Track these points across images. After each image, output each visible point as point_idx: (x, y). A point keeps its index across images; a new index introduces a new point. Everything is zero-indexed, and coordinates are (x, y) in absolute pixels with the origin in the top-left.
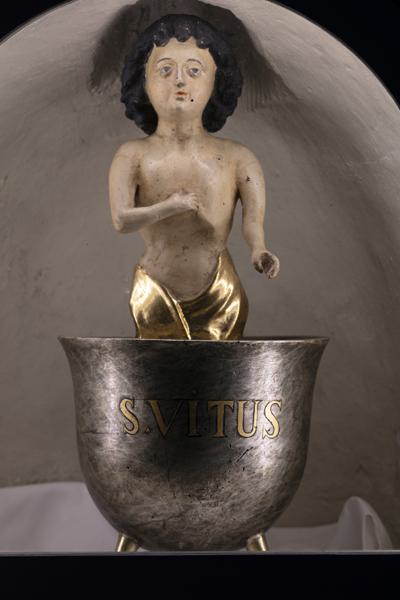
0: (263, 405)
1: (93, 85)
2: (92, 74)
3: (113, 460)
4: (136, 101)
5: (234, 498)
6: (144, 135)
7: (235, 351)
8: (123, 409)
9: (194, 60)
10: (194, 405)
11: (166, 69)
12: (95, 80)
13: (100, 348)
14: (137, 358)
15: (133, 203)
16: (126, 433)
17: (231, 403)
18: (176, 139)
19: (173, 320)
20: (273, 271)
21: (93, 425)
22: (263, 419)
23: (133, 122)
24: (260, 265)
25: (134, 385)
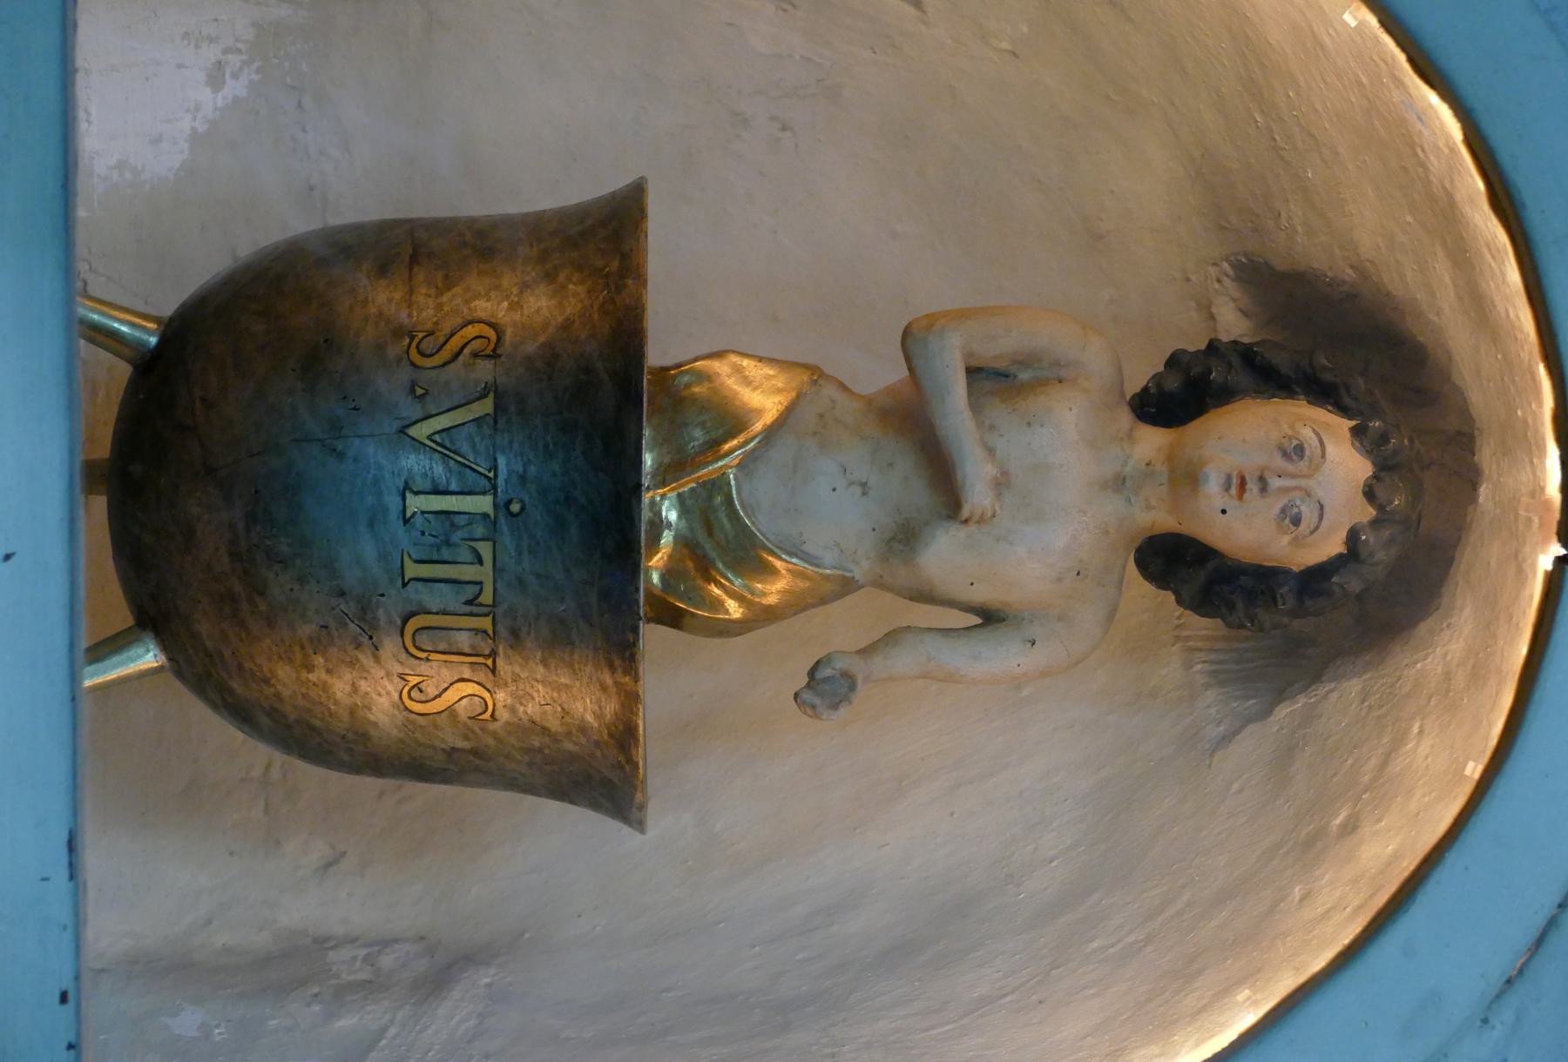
0: (481, 676)
1: (1237, 266)
2: (1267, 264)
6: (1135, 385)
8: (471, 331)
14: (599, 365)
15: (974, 363)
16: (412, 338)
21: (430, 255)
22: (447, 675)
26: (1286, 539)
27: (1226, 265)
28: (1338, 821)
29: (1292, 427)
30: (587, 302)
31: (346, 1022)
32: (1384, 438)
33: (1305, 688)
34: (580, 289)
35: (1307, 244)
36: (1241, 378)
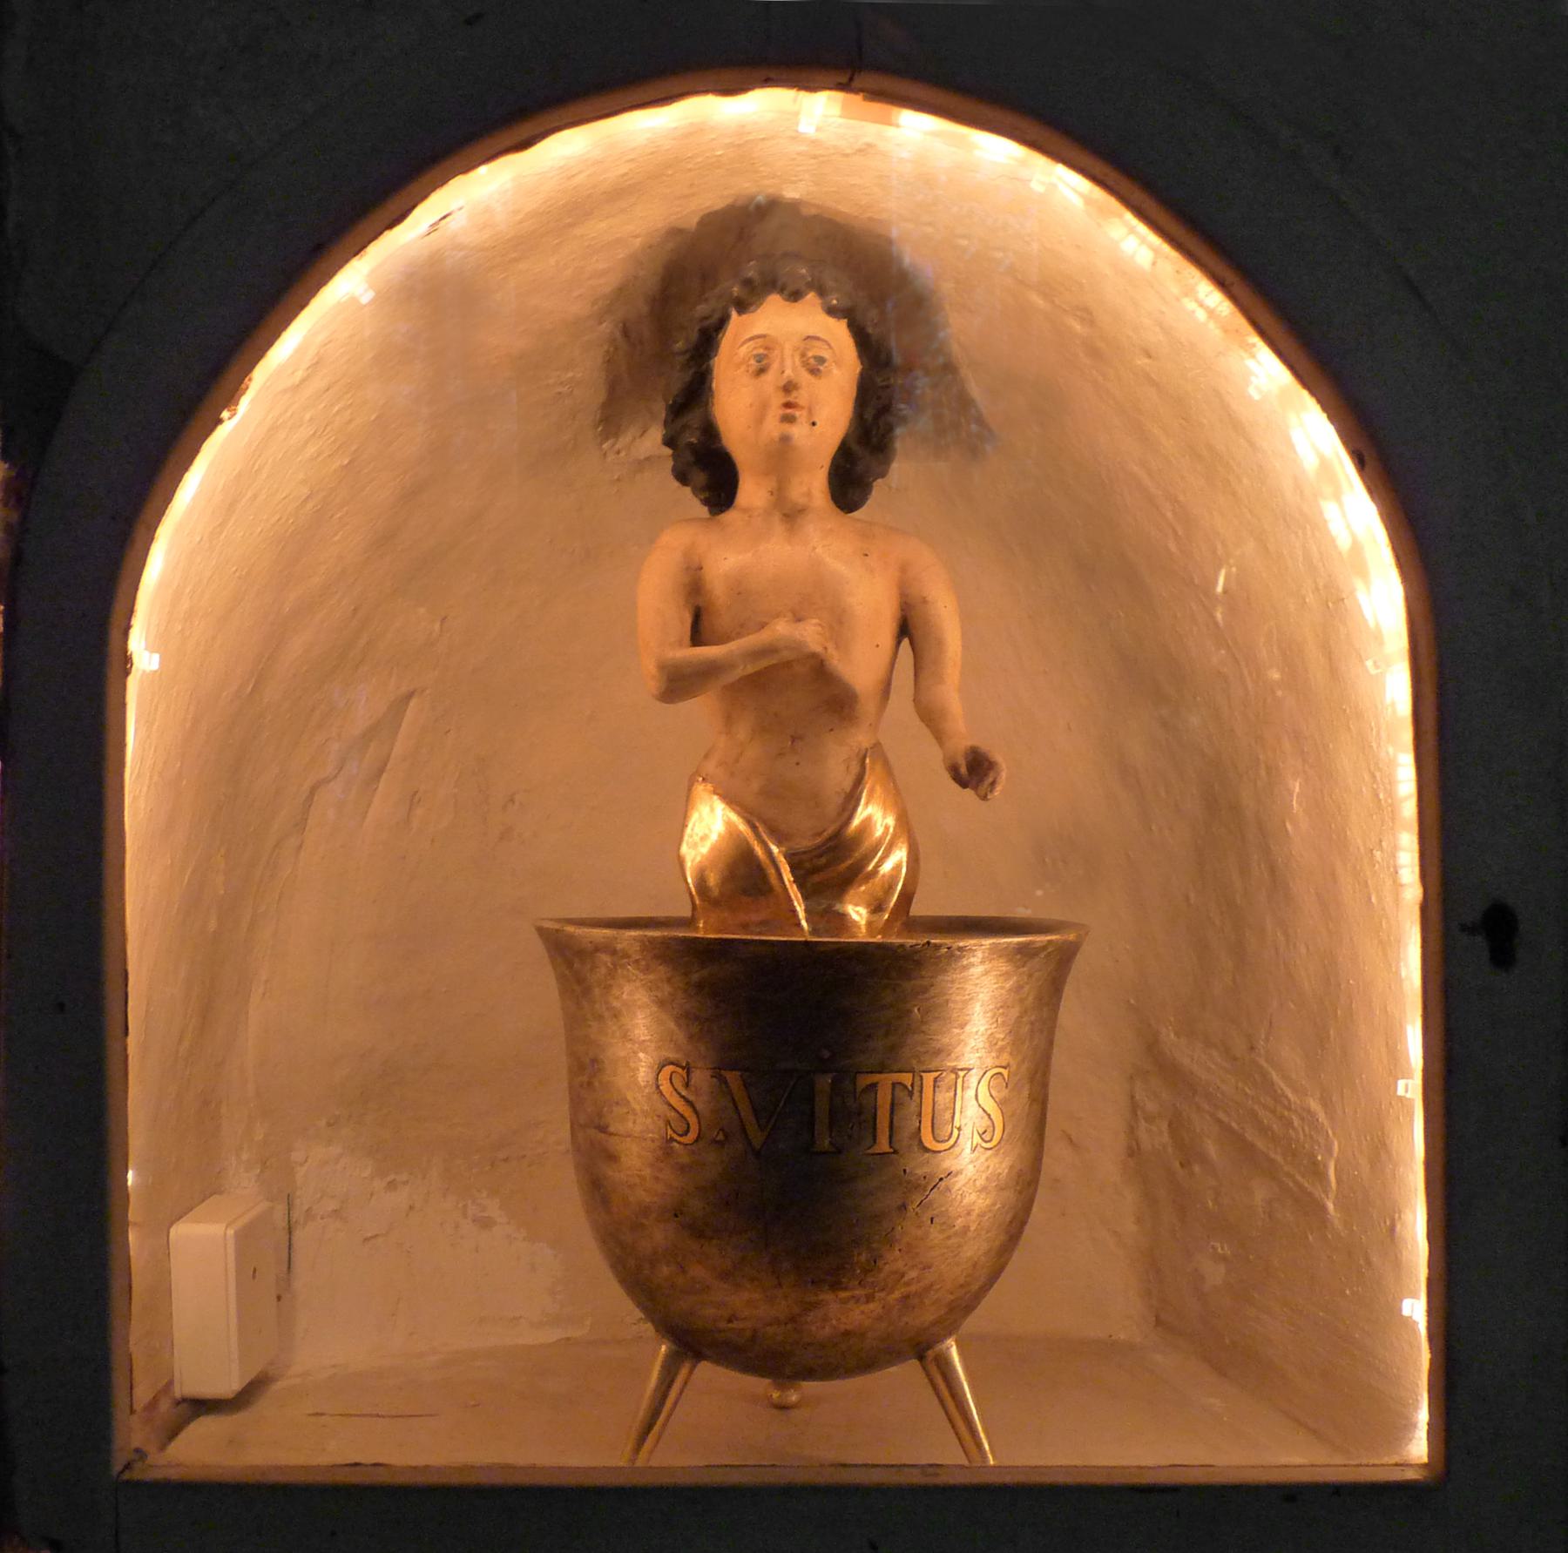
1: (606, 436)
3: (641, 1196)
4: (693, 440)
5: (908, 1284)
6: (704, 511)
7: (919, 964)
8: (665, 1087)
9: (817, 339)
10: (824, 1082)
11: (759, 358)
12: (610, 419)
13: (614, 952)
14: (695, 977)
16: (672, 1139)
17: (906, 1078)
18: (777, 518)
19: (771, 889)
20: (993, 784)
21: (600, 1115)
23: (688, 490)
24: (963, 770)
25: (691, 1037)
26: (835, 371)
27: (605, 446)
29: (738, 366)
30: (638, 984)
31: (1212, 1149)
32: (748, 283)
34: (627, 988)
35: (583, 374)
36: (693, 418)
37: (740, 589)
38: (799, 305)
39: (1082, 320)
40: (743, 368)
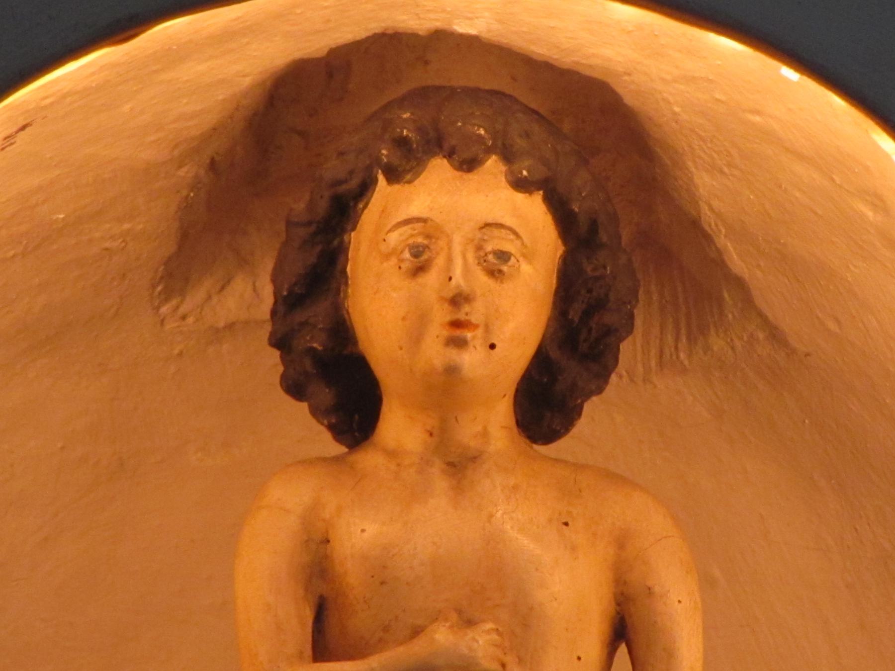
9: (500, 226)
26: (525, 268)
27: (164, 309)
28: (870, 214)
29: (387, 257)
32: (402, 143)
33: (708, 237)
36: (317, 312)
37: (382, 574)
38: (474, 177)
39: (874, 207)
40: (394, 261)
